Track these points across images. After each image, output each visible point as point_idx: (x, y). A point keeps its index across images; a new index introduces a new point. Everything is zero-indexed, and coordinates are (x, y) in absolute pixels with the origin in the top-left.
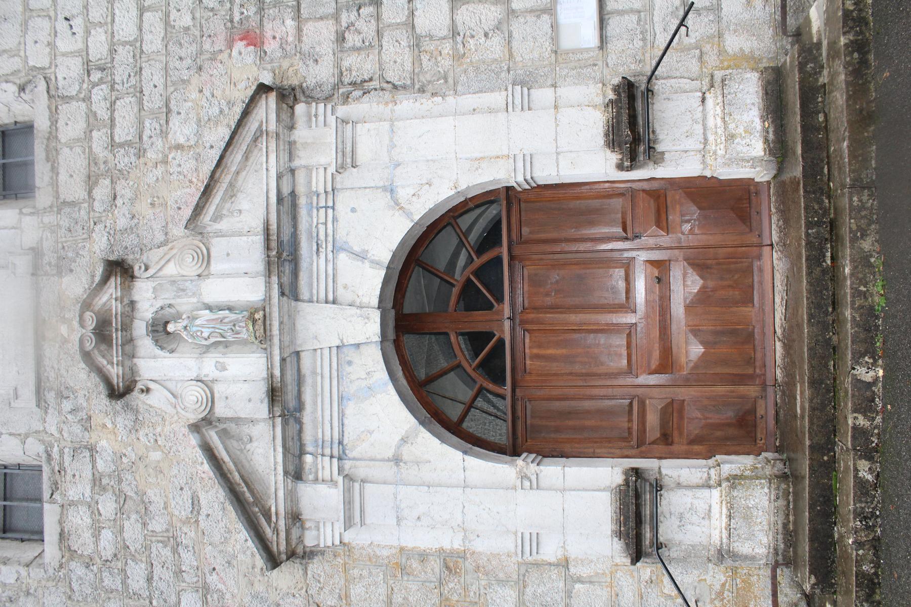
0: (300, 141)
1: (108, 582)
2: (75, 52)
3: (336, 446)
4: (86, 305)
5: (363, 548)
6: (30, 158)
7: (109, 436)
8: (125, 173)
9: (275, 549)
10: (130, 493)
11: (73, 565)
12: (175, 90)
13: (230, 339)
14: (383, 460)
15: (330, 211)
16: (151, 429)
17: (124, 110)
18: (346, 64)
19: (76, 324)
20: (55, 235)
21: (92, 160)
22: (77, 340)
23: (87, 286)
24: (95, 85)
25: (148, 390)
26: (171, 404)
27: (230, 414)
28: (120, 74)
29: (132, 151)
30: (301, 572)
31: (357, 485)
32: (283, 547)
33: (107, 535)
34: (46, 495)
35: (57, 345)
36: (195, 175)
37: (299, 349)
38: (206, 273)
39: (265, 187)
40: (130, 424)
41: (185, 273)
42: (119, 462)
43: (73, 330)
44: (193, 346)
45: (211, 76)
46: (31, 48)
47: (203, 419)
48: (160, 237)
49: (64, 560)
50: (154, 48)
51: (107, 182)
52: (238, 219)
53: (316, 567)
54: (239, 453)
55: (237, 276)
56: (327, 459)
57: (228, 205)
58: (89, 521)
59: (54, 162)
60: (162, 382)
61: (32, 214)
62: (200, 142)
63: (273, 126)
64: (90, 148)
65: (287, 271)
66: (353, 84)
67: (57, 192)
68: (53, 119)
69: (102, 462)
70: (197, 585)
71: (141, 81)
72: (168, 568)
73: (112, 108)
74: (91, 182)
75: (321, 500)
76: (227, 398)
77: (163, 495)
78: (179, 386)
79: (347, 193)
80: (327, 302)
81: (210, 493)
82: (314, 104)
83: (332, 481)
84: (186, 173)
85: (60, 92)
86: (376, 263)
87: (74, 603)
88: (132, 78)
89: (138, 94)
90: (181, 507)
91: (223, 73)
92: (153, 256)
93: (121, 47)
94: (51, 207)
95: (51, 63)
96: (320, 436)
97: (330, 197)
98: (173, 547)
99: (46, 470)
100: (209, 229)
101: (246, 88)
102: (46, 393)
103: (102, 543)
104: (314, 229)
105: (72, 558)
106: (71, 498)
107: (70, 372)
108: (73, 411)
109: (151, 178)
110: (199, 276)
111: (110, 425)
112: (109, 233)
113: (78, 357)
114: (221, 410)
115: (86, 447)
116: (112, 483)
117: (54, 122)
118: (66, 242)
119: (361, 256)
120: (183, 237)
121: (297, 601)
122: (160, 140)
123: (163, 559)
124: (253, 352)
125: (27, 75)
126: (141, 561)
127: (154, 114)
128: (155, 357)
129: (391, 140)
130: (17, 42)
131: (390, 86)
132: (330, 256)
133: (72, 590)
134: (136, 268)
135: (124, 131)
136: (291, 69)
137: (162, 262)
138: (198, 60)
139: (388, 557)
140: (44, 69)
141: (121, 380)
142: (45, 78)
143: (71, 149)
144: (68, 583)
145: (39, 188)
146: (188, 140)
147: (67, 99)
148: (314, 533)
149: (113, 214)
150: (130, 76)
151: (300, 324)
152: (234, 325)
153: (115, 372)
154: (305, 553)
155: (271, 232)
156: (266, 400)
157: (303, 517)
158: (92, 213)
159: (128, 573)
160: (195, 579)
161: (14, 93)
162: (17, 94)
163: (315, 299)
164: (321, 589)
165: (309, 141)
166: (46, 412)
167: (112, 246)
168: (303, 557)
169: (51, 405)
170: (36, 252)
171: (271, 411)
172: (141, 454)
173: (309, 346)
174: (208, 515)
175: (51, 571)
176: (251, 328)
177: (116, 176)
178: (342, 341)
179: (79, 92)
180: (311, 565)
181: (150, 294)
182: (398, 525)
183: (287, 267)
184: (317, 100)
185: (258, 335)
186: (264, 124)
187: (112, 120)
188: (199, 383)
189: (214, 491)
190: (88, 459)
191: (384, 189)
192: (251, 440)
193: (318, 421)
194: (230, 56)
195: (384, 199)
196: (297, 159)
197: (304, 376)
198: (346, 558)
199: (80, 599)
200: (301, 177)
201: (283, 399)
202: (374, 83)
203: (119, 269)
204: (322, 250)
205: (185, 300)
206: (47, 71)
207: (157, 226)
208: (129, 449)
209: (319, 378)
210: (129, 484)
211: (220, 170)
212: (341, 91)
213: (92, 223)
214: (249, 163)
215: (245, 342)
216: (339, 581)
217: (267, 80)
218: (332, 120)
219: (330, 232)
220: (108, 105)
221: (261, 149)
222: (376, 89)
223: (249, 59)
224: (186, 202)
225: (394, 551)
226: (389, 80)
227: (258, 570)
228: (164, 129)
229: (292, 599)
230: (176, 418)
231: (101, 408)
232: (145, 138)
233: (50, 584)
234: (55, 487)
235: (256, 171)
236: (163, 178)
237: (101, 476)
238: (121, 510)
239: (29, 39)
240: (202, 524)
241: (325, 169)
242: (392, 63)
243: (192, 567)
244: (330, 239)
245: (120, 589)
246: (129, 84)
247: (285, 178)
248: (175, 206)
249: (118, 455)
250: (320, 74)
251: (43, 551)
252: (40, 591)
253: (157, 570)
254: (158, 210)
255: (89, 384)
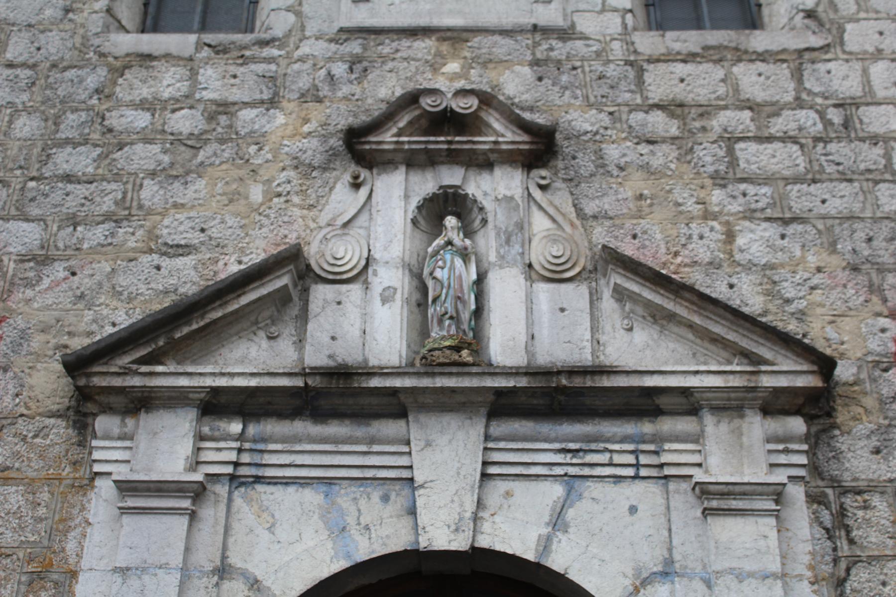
0: (745, 424)
1: (71, 118)
2: (870, 86)
3: (253, 471)
4: (487, 100)
5: (83, 509)
6: (708, 24)
7: (291, 128)
8: (689, 158)
9: (96, 369)
10: (201, 156)
11: (102, 72)
12: (819, 232)
13: (431, 311)
14: (225, 548)
15: (630, 472)
16: (297, 188)
17: (785, 156)
18: (876, 500)
19: (461, 84)
20: (594, 56)
21: (706, 111)
22: (437, 86)
23: (516, 100)
24: (822, 114)
25: (356, 185)
26: (334, 219)
27: (314, 306)
28: (839, 150)
29: (722, 168)
30: (55, 407)
31: (186, 503)
32: (97, 381)
33: (142, 120)
34: (209, 38)
35: (430, 58)
36: (687, 261)
37: (410, 418)
38: (534, 276)
39: (669, 369)
40: (306, 157)
41: (534, 243)
42: (250, 140)
43: (451, 80)
44: (422, 253)
45: (845, 286)
46: (871, 27)
47: (308, 266)
48: (590, 208)
49: (110, 59)
50: (883, 200)
51: (674, 131)
52: (618, 325)
53: (60, 431)
54: (253, 318)
55: (529, 323)
56: (232, 456)
57: (640, 310)
58: (166, 95)
59: (703, 57)
60: (368, 207)
61: (625, 25)
62: (738, 269)
63: (767, 382)
64: (726, 107)
65: (535, 402)
66: (842, 512)
67: (658, 61)
68: (767, 56)
69: (253, 116)
70: (52, 247)
71: (831, 180)
72: (83, 205)
73: (786, 139)
74: (673, 108)
75: (168, 447)
76: (339, 303)
77: (196, 202)
78: (362, 231)
79: (660, 500)
80: (485, 464)
81: (193, 273)
82: (805, 447)
83: (198, 463)
84: (690, 247)
85: (808, 66)
86: (546, 544)
87: (45, 71)
88: (836, 168)
89: (810, 176)
90: (176, 228)
91: (850, 304)
92: (562, 198)
93: (882, 152)
94: (635, 52)
95: (850, 53)
96: (272, 447)
97: (654, 472)
98: (114, 213)
99: (248, 38)
100: (602, 282)
101: (828, 340)
102: (360, 41)
103: (130, 114)
104: (601, 446)
105: (112, 69)
106: (202, 71)
107: (389, 75)
108: (330, 76)
109: (681, 194)
110: (530, 266)
111: (306, 129)
112: (597, 133)
113: (411, 86)
114: (321, 293)
115: (276, 94)
116: (219, 130)
117: (763, 57)
118: (583, 72)
119: (558, 521)
120: (590, 242)
121: (8, 399)
122: (741, 209)
123: (98, 199)
124: (409, 346)
125: (832, 22)
126: (97, 168)
127: (780, 200)
128: (407, 197)
129: (751, 575)
130: (879, 8)
131: (843, 574)
132: (559, 471)
133: (65, 69)
134: (544, 172)
135: (751, 155)
136: (860, 410)
137: (551, 211)
138: (869, 266)
139: (63, 550)
140: (842, 43)
141: (374, 147)
142: (828, 45)
143: (723, 81)
144: (76, 63)
145: (663, 36)
146: (742, 251)
147: (798, 76)
148: (116, 431)
149: (625, 139)
150: (838, 164)
151: (452, 421)
152: (451, 318)
153: (388, 138)
154: (85, 415)
155: (597, 378)
156: (332, 363)
157: (143, 415)
158: (626, 109)
159: (82, 149)
160: (61, 245)
161: (803, 4)
162: (801, 7)
163: (491, 445)
164: (24, 439)
165: (745, 439)
166: (331, 41)
167: (578, 137)
168: (77, 412)
169: (342, 48)
170: (566, 34)
171: (316, 372)
172: (261, 172)
173: (415, 434)
174: (158, 268)
175: (96, 41)
176: (447, 343)
177: (684, 145)
178: (422, 486)
179: (810, 92)
180: (64, 424)
181: (502, 191)
182: (116, 570)
183: (541, 402)
184: (811, 453)
185: (436, 353)
186: (769, 368)
187: (770, 139)
188: (363, 262)
189: (196, 279)
190: (258, 96)
191: (669, 561)
192: (270, 338)
193: (299, 445)
194: (879, 314)
195: (651, 558)
196: (715, 419)
197: (368, 425)
198: (68, 482)
199: (51, 80)
200: (684, 425)
201: (337, 396)
202: (846, 547)
203: (540, 149)
204: (568, 458)
205: (493, 243)
206: (838, 49)
207: (607, 204)
208: (269, 156)
209: (364, 448)
210: (215, 154)
211: (695, 299)
212: (829, 491)
213: (612, 109)
214: (707, 344)
215: (424, 333)
216: (34, 468)
217: (844, 372)
218: (780, 477)
219: (598, 471)
220: (791, 133)
221: (729, 362)
222: (835, 549)
223: (874, 345)
224: (644, 247)
225: (72, 560)
226: (853, 571)
227: (65, 340)
228: (758, 215)
229: (12, 391)
230: (313, 225)
231: (334, 117)
232: (743, 186)
233: (78, 40)
234: (219, 50)
235: (694, 354)
236: (681, 213)
237: (232, 115)
238: (178, 140)
239: (884, 25)
240: (145, 259)
241: (700, 465)
242: (882, 577)
243: (81, 241)
244: (587, 471)
245: (58, 136)
246: (825, 164)
247: (682, 400)
248: (638, 231)
249: (261, 139)
250: (858, 460)
251: (128, 32)
252: (68, 26)
253: (81, 190)
254: (631, 205)
255: (370, 101)
